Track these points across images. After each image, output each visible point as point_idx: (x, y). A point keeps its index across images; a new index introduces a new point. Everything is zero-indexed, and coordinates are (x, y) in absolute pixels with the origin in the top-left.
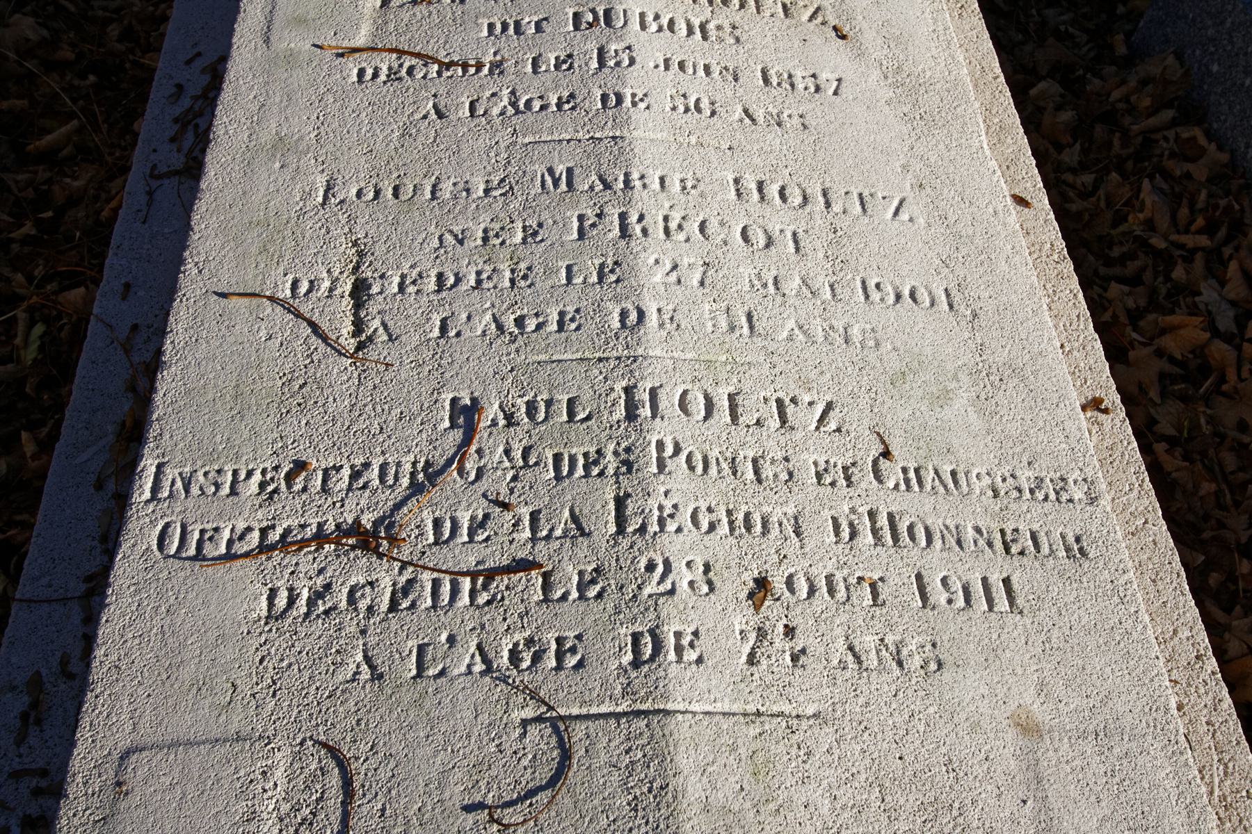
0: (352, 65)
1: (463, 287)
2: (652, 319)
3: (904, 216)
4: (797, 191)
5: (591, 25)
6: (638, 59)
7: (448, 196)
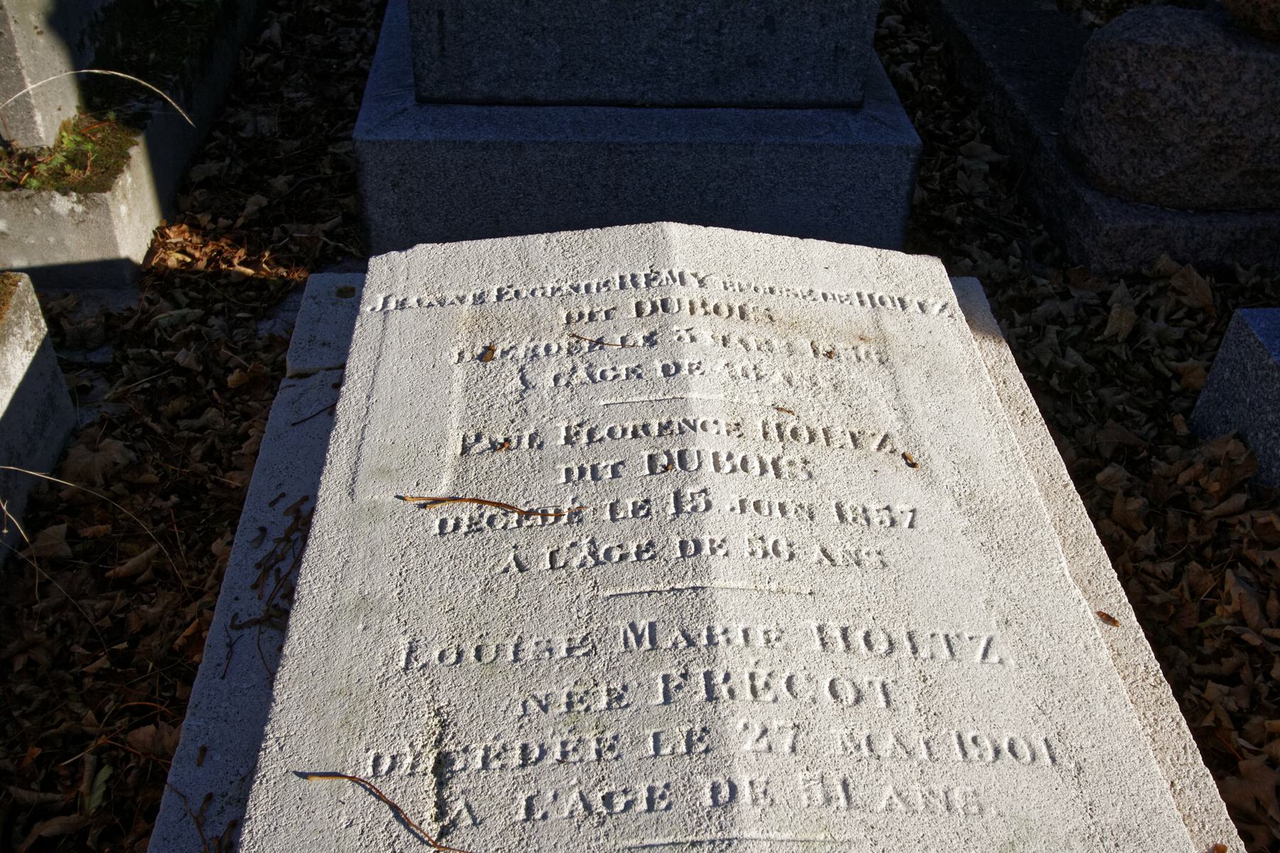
0: (433, 517)
1: (549, 761)
2: (745, 794)
3: (993, 658)
4: (882, 637)
5: (666, 468)
6: (714, 503)
7: (531, 657)
